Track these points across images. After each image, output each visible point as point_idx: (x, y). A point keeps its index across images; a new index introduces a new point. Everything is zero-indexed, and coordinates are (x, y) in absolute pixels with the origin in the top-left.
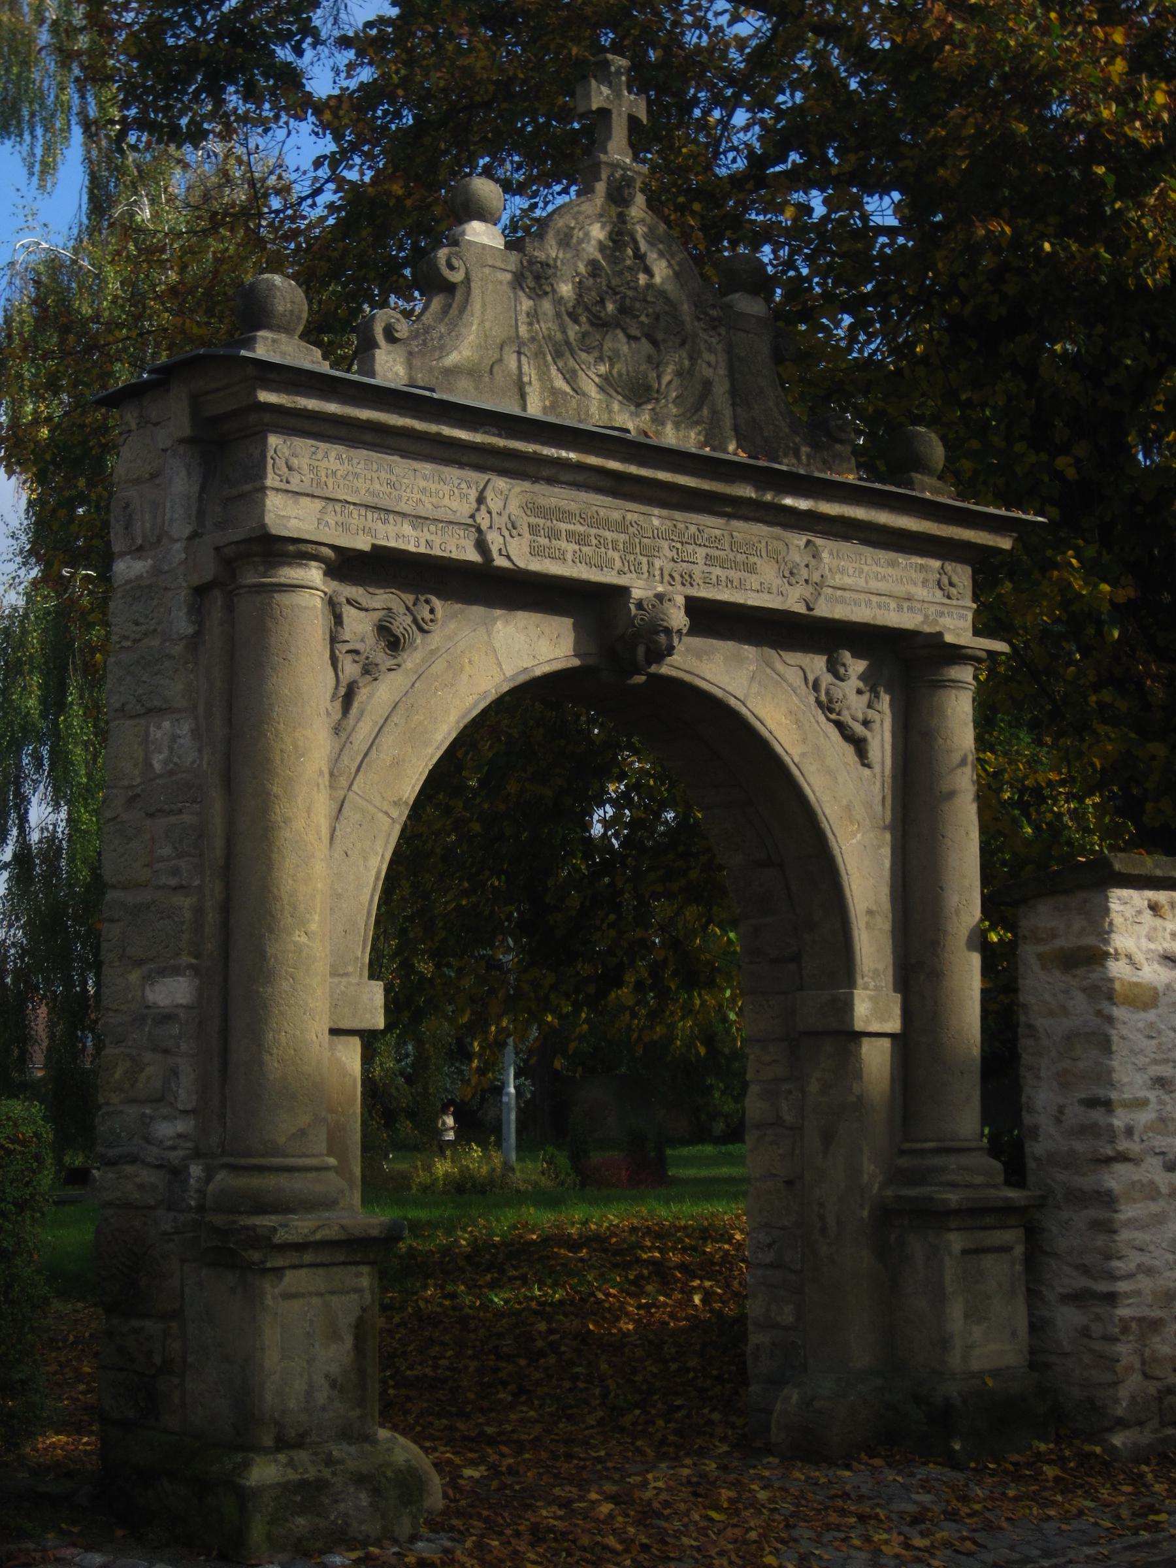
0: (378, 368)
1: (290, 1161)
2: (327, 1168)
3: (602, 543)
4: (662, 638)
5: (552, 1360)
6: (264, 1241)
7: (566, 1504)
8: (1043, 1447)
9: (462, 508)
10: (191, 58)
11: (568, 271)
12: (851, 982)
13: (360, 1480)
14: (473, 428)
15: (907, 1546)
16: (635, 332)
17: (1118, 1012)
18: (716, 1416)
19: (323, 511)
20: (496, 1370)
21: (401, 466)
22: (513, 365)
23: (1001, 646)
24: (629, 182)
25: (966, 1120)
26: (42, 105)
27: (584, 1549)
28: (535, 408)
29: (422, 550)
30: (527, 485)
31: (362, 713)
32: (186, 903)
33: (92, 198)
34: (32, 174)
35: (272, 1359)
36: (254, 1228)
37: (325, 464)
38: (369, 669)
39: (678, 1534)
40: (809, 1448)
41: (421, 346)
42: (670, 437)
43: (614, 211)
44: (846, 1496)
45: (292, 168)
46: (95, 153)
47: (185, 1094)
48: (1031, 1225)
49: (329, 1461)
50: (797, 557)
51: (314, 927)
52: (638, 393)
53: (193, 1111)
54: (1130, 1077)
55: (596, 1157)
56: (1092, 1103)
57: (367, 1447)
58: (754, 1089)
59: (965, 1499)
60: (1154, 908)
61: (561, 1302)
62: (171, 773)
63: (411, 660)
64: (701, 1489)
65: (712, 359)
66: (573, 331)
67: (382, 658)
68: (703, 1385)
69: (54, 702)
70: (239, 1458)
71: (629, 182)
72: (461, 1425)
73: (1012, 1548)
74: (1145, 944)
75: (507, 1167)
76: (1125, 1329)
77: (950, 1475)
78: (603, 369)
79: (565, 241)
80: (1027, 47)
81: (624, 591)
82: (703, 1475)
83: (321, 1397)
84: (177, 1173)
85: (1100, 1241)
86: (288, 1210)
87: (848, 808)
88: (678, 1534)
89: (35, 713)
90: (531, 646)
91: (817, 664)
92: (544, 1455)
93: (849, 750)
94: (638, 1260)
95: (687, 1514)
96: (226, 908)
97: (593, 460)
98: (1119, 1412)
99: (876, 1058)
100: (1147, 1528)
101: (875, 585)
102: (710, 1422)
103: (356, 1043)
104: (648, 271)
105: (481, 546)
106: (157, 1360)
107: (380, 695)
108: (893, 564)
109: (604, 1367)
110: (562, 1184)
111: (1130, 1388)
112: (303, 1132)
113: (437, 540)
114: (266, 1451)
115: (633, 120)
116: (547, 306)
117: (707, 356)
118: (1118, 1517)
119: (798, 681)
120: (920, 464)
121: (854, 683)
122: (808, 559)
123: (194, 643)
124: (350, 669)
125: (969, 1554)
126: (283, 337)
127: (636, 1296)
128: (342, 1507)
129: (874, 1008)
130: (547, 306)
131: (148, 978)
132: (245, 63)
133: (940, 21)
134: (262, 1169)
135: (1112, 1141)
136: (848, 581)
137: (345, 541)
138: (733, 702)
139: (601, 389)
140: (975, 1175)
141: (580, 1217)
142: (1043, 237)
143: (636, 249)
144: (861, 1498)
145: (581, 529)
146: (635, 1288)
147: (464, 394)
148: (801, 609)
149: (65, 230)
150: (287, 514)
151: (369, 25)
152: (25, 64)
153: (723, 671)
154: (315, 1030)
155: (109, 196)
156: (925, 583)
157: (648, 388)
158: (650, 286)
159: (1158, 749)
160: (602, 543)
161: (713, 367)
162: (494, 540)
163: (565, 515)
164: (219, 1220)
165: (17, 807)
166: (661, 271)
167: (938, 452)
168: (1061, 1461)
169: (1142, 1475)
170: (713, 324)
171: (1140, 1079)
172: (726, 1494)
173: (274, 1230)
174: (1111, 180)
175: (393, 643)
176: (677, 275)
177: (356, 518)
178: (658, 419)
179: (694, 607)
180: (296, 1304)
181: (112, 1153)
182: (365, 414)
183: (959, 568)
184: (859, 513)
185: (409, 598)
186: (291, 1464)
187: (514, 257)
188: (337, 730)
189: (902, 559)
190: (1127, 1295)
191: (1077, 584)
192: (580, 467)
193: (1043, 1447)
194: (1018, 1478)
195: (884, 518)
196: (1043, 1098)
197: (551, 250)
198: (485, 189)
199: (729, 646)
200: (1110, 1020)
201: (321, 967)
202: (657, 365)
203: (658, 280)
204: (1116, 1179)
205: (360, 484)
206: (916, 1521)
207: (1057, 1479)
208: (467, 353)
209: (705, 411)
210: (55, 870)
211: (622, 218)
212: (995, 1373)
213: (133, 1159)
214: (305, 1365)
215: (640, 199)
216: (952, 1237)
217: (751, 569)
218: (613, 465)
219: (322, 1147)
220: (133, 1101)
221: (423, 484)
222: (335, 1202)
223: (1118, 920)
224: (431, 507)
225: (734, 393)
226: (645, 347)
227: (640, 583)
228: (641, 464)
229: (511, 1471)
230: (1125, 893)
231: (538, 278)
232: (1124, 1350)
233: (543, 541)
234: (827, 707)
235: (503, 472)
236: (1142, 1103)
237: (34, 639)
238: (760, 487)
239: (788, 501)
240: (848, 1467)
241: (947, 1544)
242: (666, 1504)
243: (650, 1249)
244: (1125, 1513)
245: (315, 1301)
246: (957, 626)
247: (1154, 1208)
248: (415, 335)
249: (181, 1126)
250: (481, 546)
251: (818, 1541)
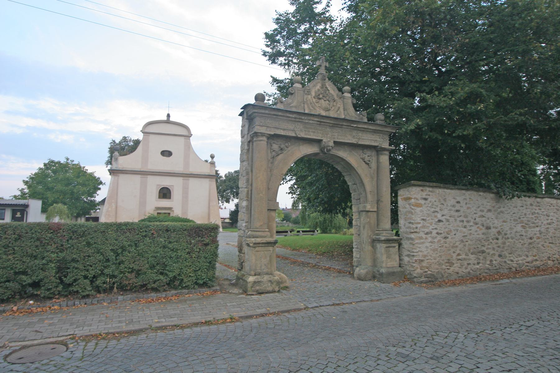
28: (306, 112)
153: (342, 153)
171: (419, 219)
214: (208, 264)
225: (344, 109)
247: (422, 241)
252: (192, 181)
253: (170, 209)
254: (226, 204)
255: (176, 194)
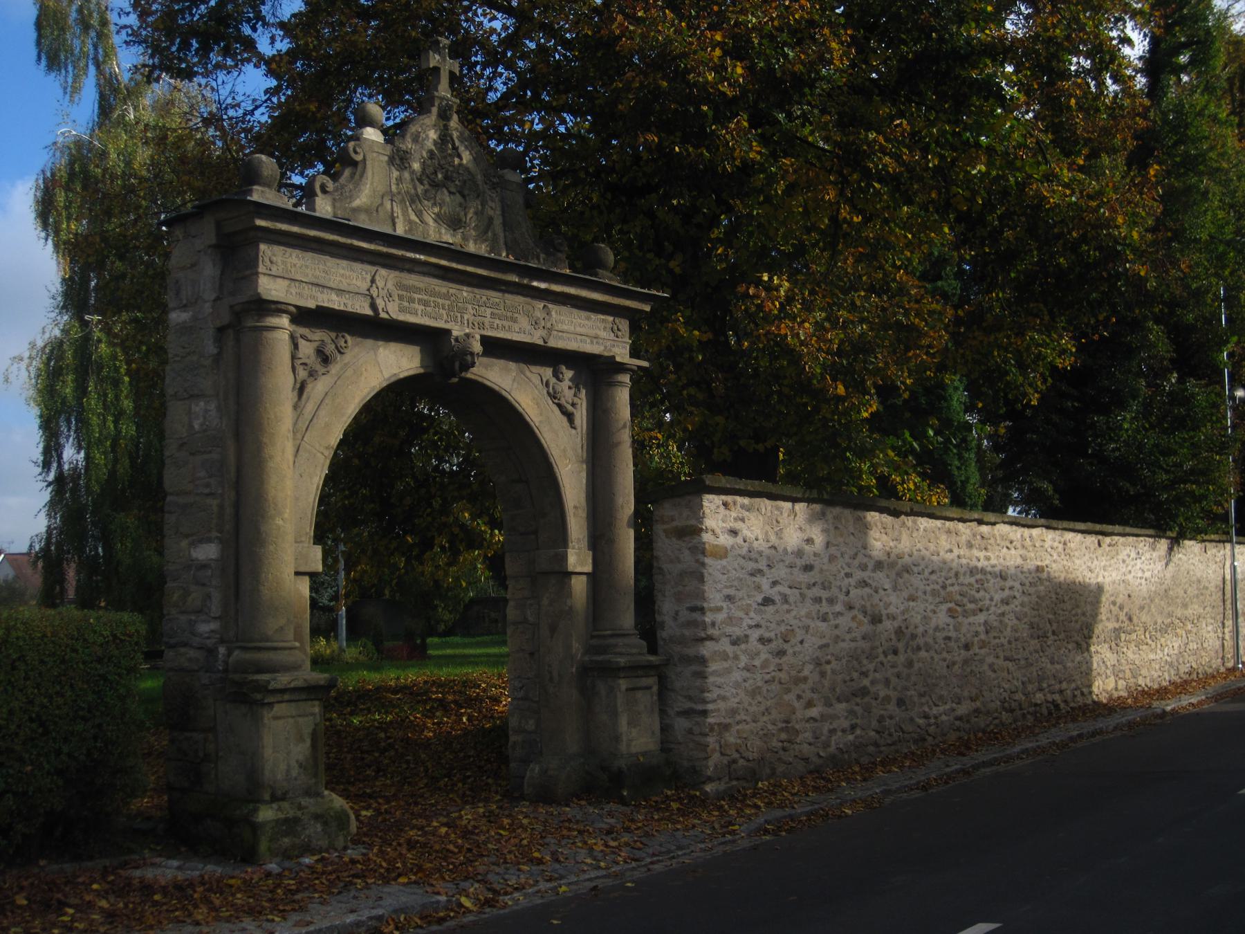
0: (317, 207)
1: (275, 644)
2: (295, 648)
3: (436, 305)
4: (469, 358)
5: (392, 753)
6: (264, 689)
7: (421, 828)
8: (669, 793)
9: (363, 285)
10: (193, 31)
11: (417, 156)
12: (566, 546)
13: (317, 817)
14: (370, 242)
15: (607, 846)
16: (453, 190)
17: (707, 560)
18: (490, 781)
19: (289, 286)
20: (363, 759)
21: (331, 262)
22: (389, 207)
23: (645, 364)
24: (450, 108)
25: (628, 619)
26: (72, 54)
27: (437, 852)
28: (400, 231)
29: (342, 308)
30: (397, 273)
31: (308, 398)
32: (214, 503)
33: (101, 107)
34: (65, 93)
35: (268, 752)
36: (257, 681)
37: (289, 260)
38: (312, 374)
39: (485, 842)
40: (545, 795)
41: (340, 197)
42: (471, 248)
43: (442, 123)
44: (569, 821)
45: (241, 93)
46: (102, 81)
47: (215, 608)
48: (661, 674)
49: (300, 807)
50: (539, 314)
51: (286, 516)
52: (455, 223)
53: (219, 618)
54: (714, 595)
55: (388, 644)
56: (694, 609)
57: (319, 799)
58: (511, 603)
59: (633, 821)
60: (725, 504)
61: (391, 722)
62: (205, 431)
63: (334, 369)
64: (491, 818)
65: (493, 205)
66: (420, 189)
67: (321, 370)
68: (484, 761)
69: (81, 390)
70: (251, 806)
71: (450, 108)
72: (351, 789)
73: (661, 845)
74: (721, 524)
75: (342, 650)
76: (712, 730)
77: (622, 808)
78: (436, 210)
79: (416, 139)
80: (669, 41)
81: (448, 332)
82: (491, 812)
83: (294, 773)
84: (211, 652)
85: (698, 683)
86: (278, 671)
87: (564, 451)
88: (485, 842)
89: (70, 398)
90: (400, 361)
91: (548, 372)
92: (402, 803)
93: (565, 419)
94: (430, 699)
95: (488, 831)
96: (237, 505)
97: (433, 260)
98: (709, 774)
99: (579, 586)
100: (729, 833)
101: (579, 330)
102: (487, 784)
103: (307, 579)
104: (460, 157)
105: (373, 306)
106: (201, 754)
107: (318, 388)
108: (588, 319)
109: (423, 756)
110: (371, 659)
111: (714, 760)
112: (282, 628)
113: (350, 303)
114: (266, 802)
115: (452, 73)
116: (406, 175)
117: (490, 203)
118: (714, 828)
119: (538, 382)
120: (603, 265)
121: (567, 383)
122: (544, 315)
123: (217, 358)
124: (302, 374)
125: (639, 849)
126: (267, 189)
127: (432, 718)
128: (307, 832)
129: (578, 559)
130: (406, 175)
131: (193, 544)
132: (223, 37)
133: (621, 25)
134: (260, 649)
135: (705, 629)
136: (565, 327)
137: (301, 303)
138: (504, 393)
139: (435, 221)
140: (631, 649)
141: (392, 676)
142: (674, 143)
143: (453, 144)
144: (577, 822)
145: (425, 297)
146: (430, 714)
147: (363, 222)
148: (541, 342)
149: (85, 124)
150: (270, 287)
151: (294, 15)
152: (63, 30)
153: (498, 375)
154: (288, 571)
155: (110, 104)
156: (605, 328)
157: (460, 221)
158: (460, 165)
159: (720, 419)
160: (436, 305)
161: (494, 210)
162: (380, 303)
163: (418, 290)
164: (237, 677)
165: (56, 450)
166: (466, 157)
167: (610, 258)
168: (680, 800)
169: (722, 806)
170: (494, 186)
172: (506, 821)
173: (268, 682)
174: (711, 114)
175: (325, 359)
176: (475, 159)
177: (307, 290)
178: (465, 238)
179: (485, 340)
180: (281, 722)
181: (173, 641)
182: (312, 233)
183: (623, 321)
184: (572, 291)
185: (333, 335)
186: (279, 809)
187: (389, 147)
188: (295, 407)
189: (593, 316)
190: (712, 711)
191: (682, 331)
192: (426, 263)
193: (669, 793)
194: (658, 810)
195: (584, 293)
196: (667, 607)
197: (408, 144)
198: (374, 109)
199: (502, 362)
200: (703, 564)
201: (290, 538)
202: (465, 208)
203: (465, 162)
204: (707, 649)
205: (308, 271)
206: (609, 832)
207: (678, 809)
208: (364, 200)
209: (490, 234)
210: (76, 485)
211: (446, 127)
212: (644, 754)
213: (185, 645)
215: (455, 117)
216: (621, 681)
217: (515, 320)
218: (444, 263)
219: (291, 636)
220: (183, 612)
221: (342, 271)
222: (300, 666)
223: (707, 511)
224: (346, 285)
225: (505, 224)
226: (458, 198)
227: (457, 327)
228: (458, 262)
229: (386, 811)
230: (711, 497)
231: (401, 159)
232: (711, 740)
233: (406, 304)
234: (553, 396)
235: (385, 266)
236: (719, 609)
237: (69, 354)
238: (520, 275)
239: (535, 284)
240: (567, 805)
241: (627, 844)
242: (475, 827)
243: (437, 693)
244: (717, 826)
245: (291, 720)
246: (622, 353)
247: (726, 665)
248: (336, 190)
249: (214, 626)
250: (373, 306)
251: (559, 844)
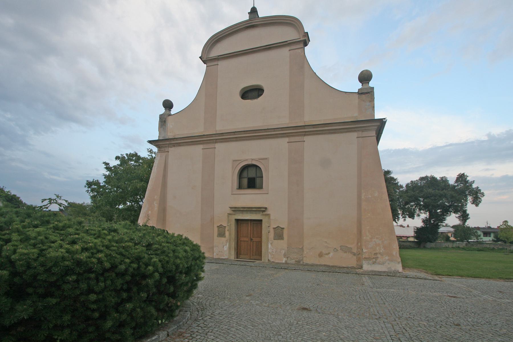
252: (311, 142)
253: (262, 210)
254: (408, 220)
255: (275, 178)
